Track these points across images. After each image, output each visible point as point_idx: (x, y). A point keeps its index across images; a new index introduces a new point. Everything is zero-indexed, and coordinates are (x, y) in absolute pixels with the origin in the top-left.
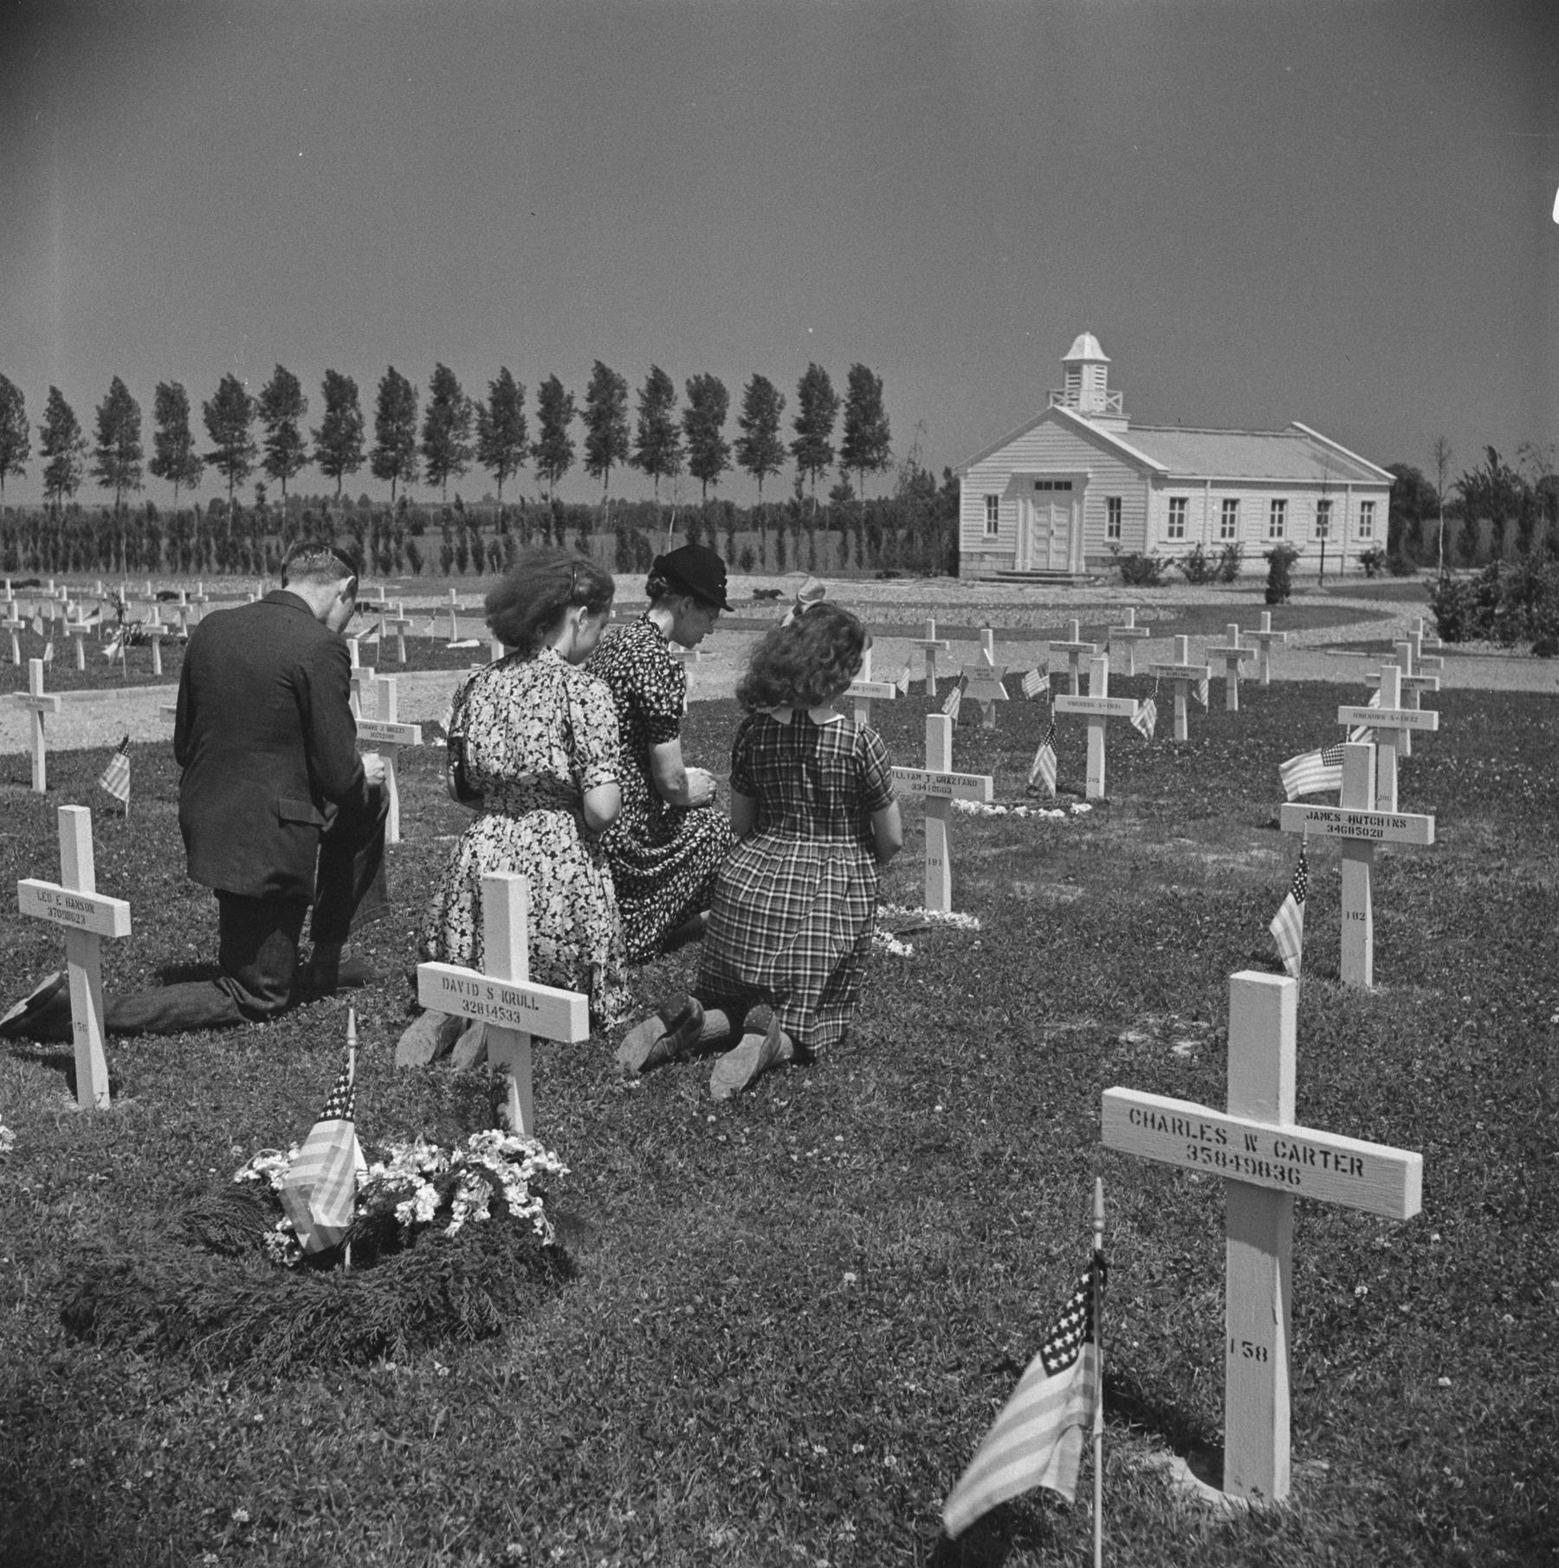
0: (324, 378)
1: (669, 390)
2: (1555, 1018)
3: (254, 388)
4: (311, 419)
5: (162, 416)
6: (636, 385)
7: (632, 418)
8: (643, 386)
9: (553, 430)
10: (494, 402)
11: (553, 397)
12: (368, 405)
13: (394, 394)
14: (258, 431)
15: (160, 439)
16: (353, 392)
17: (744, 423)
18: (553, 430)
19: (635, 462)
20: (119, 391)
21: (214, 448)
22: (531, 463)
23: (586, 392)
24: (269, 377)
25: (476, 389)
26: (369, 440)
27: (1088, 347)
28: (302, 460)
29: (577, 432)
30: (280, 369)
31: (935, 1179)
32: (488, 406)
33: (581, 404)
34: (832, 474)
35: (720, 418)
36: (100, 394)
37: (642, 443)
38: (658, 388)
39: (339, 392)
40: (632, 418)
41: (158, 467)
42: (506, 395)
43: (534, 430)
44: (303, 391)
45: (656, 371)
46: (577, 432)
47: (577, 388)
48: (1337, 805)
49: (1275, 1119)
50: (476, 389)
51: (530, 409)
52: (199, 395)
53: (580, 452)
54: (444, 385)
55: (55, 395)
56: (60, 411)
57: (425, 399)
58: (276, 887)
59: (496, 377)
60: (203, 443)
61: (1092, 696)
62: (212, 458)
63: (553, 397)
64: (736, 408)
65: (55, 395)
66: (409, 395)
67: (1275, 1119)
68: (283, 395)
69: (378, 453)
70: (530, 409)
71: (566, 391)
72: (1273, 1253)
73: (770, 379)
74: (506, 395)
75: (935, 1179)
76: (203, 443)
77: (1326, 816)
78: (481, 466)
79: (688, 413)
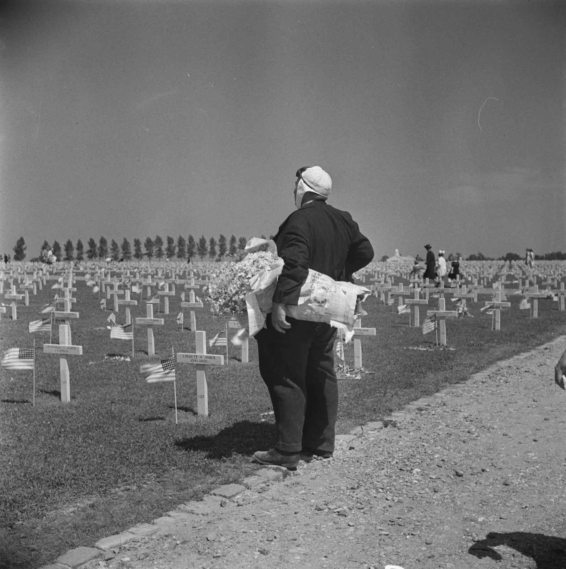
1: (235, 240)
2: (564, 409)
3: (153, 239)
4: (165, 246)
7: (228, 246)
9: (212, 248)
10: (200, 242)
11: (212, 241)
12: (176, 243)
13: (181, 241)
15: (136, 250)
16: (173, 241)
18: (212, 248)
22: (208, 254)
23: (218, 240)
25: (197, 240)
27: (397, 250)
28: (163, 254)
29: (217, 248)
31: (325, 478)
32: (199, 243)
36: (99, 238)
40: (228, 246)
42: (203, 241)
43: (209, 249)
45: (233, 236)
46: (217, 248)
47: (217, 239)
48: (195, 353)
50: (197, 240)
51: (208, 244)
52: (143, 241)
54: (191, 239)
55: (113, 241)
56: (114, 244)
58: (327, 347)
59: (201, 237)
60: (144, 250)
61: (191, 303)
62: (146, 254)
63: (212, 241)
65: (113, 241)
66: (184, 240)
69: (178, 253)
70: (208, 244)
74: (203, 241)
75: (325, 478)
76: (144, 250)
77: (191, 356)
78: (198, 256)
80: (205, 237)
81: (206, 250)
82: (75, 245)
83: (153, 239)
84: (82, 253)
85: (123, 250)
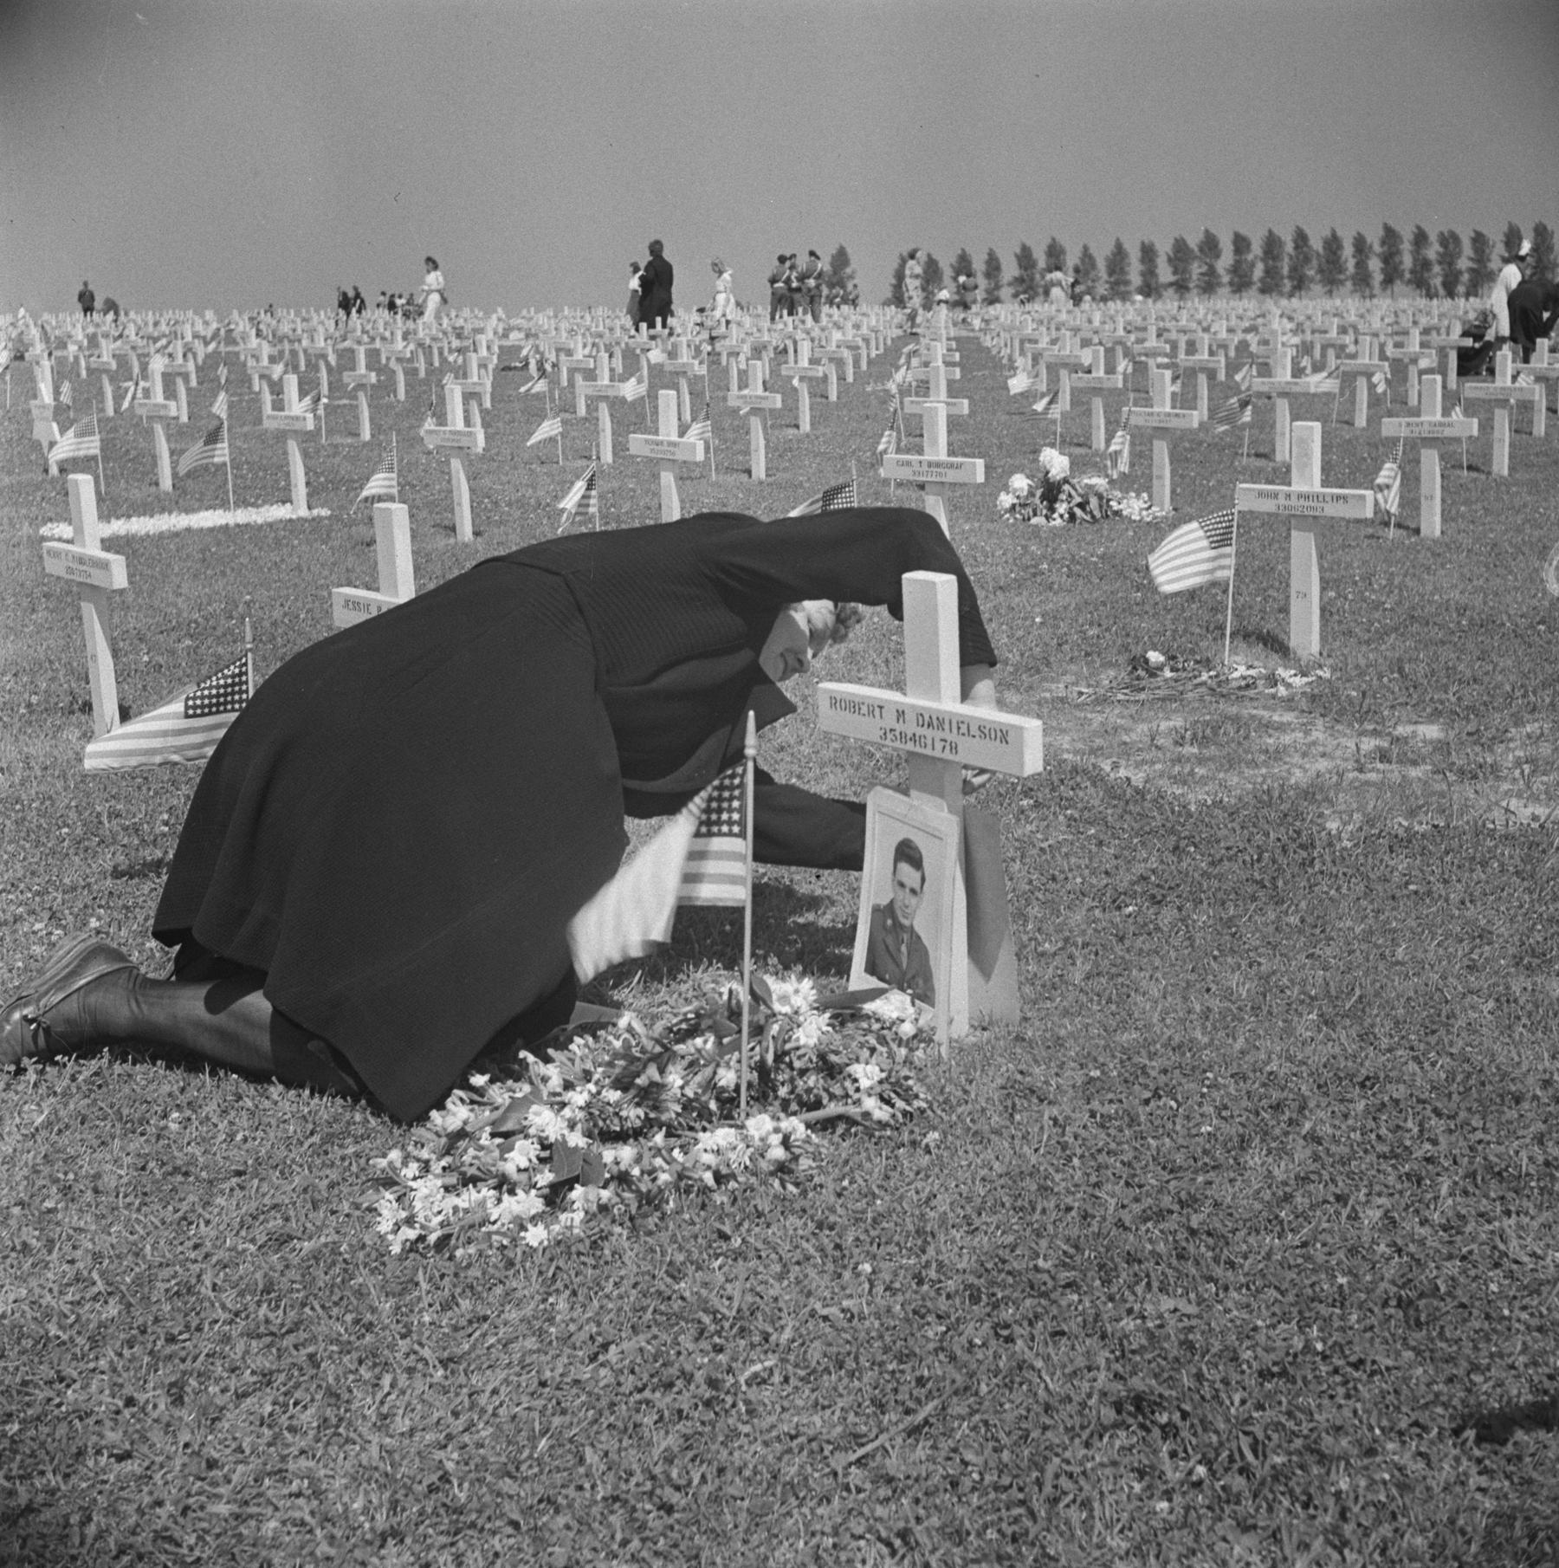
0: (1018, 251)
3: (1193, 241)
4: (1010, 270)
5: (1143, 261)
6: (1407, 234)
7: (1407, 261)
8: (1411, 237)
9: (1361, 264)
11: (1360, 245)
12: (1257, 249)
13: (1272, 245)
14: (1196, 269)
17: (1471, 259)
19: (1409, 282)
20: (1335, 237)
21: (1172, 278)
22: (1349, 284)
24: (1201, 236)
26: (1258, 272)
30: (1270, 232)
33: (1377, 248)
34: (189, 338)
35: (1459, 254)
37: (1412, 272)
38: (1421, 238)
39: (1241, 244)
41: (1140, 291)
43: (1351, 265)
44: (1221, 245)
45: (1418, 228)
46: (1375, 265)
47: (1374, 238)
49: (937, 696)
51: (1348, 251)
52: (1164, 248)
53: (1378, 277)
54: (1301, 238)
55: (1086, 248)
57: (1289, 247)
63: (1360, 245)
64: (1467, 249)
67: (937, 696)
68: (1210, 245)
70: (1348, 251)
71: (1369, 240)
72: (942, 796)
73: (1485, 232)
74: (1333, 244)
76: (1165, 274)
79: (1438, 253)
80: (1339, 233)
81: (1341, 270)
82: (1407, 234)
83: (1193, 241)
84: (998, 287)
85: (1110, 275)
